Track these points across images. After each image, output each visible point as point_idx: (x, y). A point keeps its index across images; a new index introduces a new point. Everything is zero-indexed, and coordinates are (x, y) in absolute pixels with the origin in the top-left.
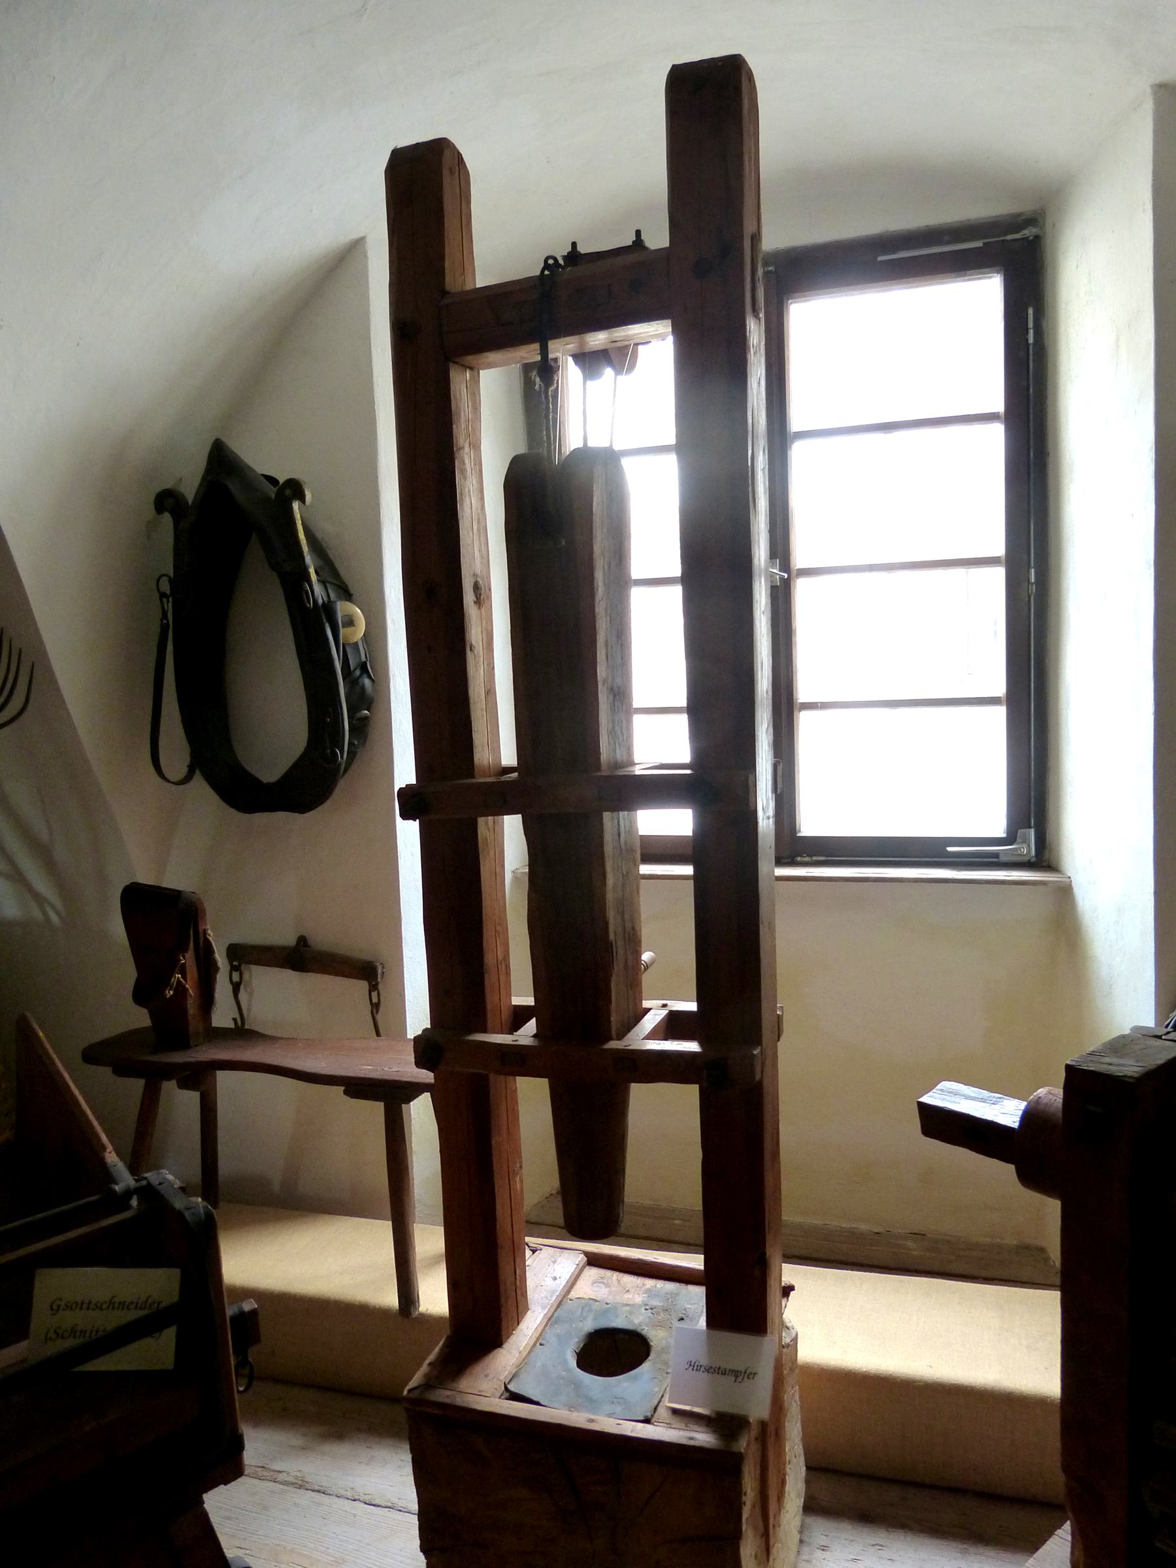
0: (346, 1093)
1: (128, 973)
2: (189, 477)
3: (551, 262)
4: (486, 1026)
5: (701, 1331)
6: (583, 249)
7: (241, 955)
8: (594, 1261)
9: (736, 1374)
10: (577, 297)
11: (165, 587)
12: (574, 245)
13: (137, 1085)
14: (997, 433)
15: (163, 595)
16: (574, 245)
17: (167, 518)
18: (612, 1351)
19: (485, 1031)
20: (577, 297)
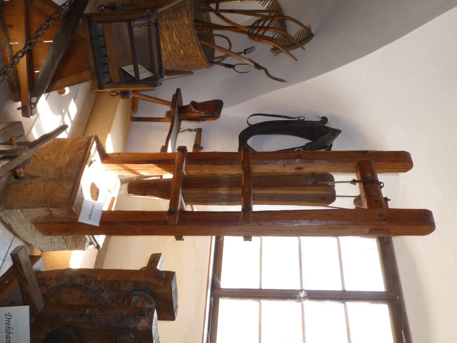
0: (163, 146)
1: (199, 100)
2: (331, 124)
3: (382, 185)
4: (188, 164)
5: (102, 208)
6: (389, 202)
7: (199, 131)
8: (113, 199)
9: (90, 216)
10: (370, 186)
11: (301, 118)
12: (390, 200)
13: (170, 100)
14: (340, 289)
15: (299, 118)
16: (390, 200)
17: (320, 120)
18: (95, 192)
19: (186, 164)
20: (370, 186)
